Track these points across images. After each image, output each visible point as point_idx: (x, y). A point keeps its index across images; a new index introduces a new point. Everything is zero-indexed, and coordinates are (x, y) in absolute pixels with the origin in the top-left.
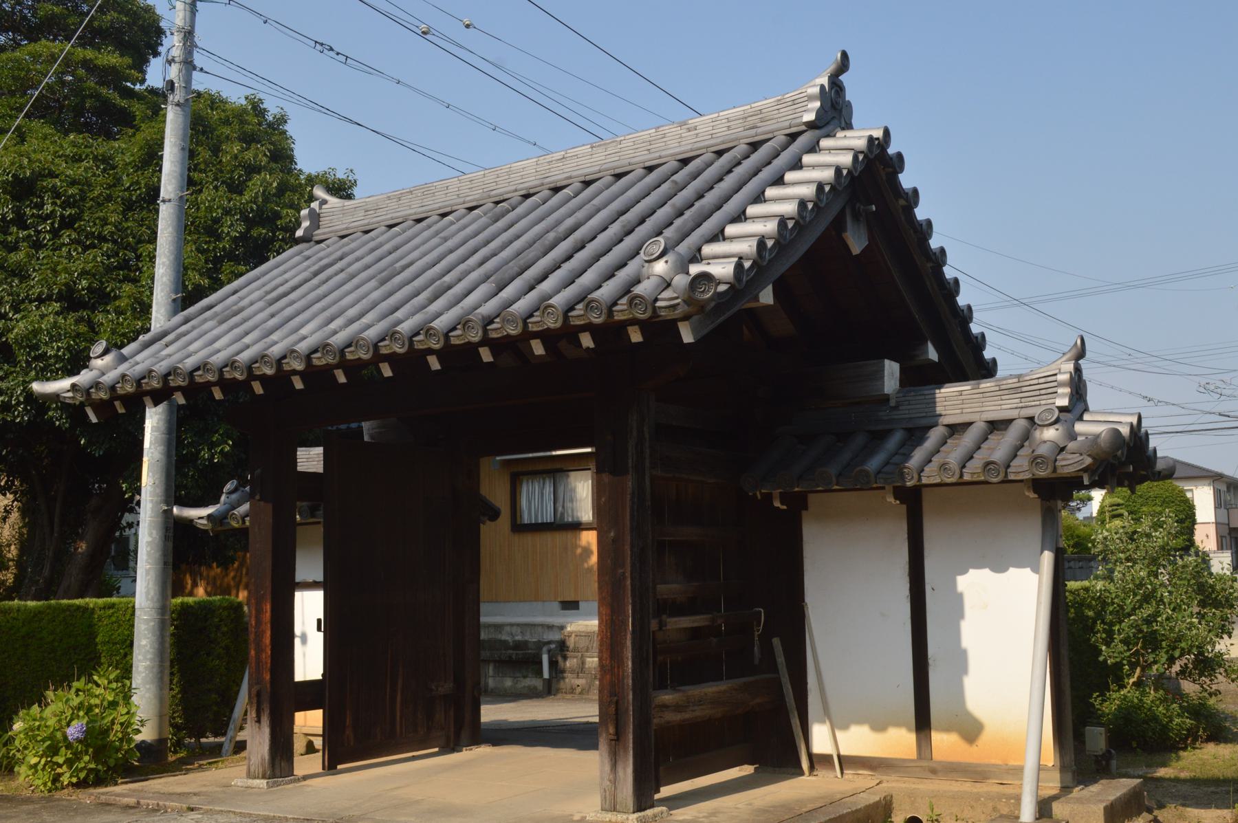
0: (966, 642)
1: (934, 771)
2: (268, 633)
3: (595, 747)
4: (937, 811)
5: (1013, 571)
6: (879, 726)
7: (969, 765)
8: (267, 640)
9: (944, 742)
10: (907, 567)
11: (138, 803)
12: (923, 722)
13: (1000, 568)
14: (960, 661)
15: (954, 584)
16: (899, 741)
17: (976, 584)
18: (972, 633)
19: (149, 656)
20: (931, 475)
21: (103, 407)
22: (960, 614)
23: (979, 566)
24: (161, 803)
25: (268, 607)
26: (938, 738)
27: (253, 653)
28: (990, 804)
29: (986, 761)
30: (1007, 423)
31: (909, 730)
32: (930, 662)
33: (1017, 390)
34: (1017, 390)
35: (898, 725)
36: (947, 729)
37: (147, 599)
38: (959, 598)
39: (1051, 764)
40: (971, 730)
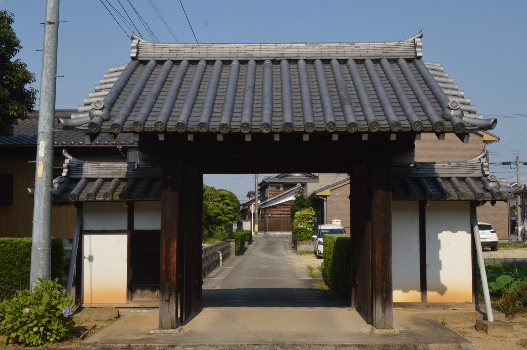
0: (441, 257)
1: (428, 306)
2: (175, 257)
3: (349, 305)
4: (445, 321)
5: (459, 232)
6: (405, 290)
7: (442, 303)
8: (174, 259)
9: (432, 295)
10: (419, 230)
11: (129, 346)
12: (423, 288)
13: (454, 231)
14: (438, 265)
15: (437, 236)
16: (414, 296)
17: (446, 237)
18: (443, 254)
19: (45, 270)
20: (83, 197)
21: (400, 134)
22: (439, 247)
23: (447, 230)
24: (148, 345)
25: (175, 244)
26: (429, 294)
27: (164, 267)
28: (465, 317)
29: (447, 302)
30: (110, 180)
31: (418, 291)
32: (427, 266)
33: (465, 167)
34: (465, 167)
35: (413, 289)
36: (433, 290)
37: (44, 238)
38: (439, 242)
39: (471, 301)
40: (442, 290)
